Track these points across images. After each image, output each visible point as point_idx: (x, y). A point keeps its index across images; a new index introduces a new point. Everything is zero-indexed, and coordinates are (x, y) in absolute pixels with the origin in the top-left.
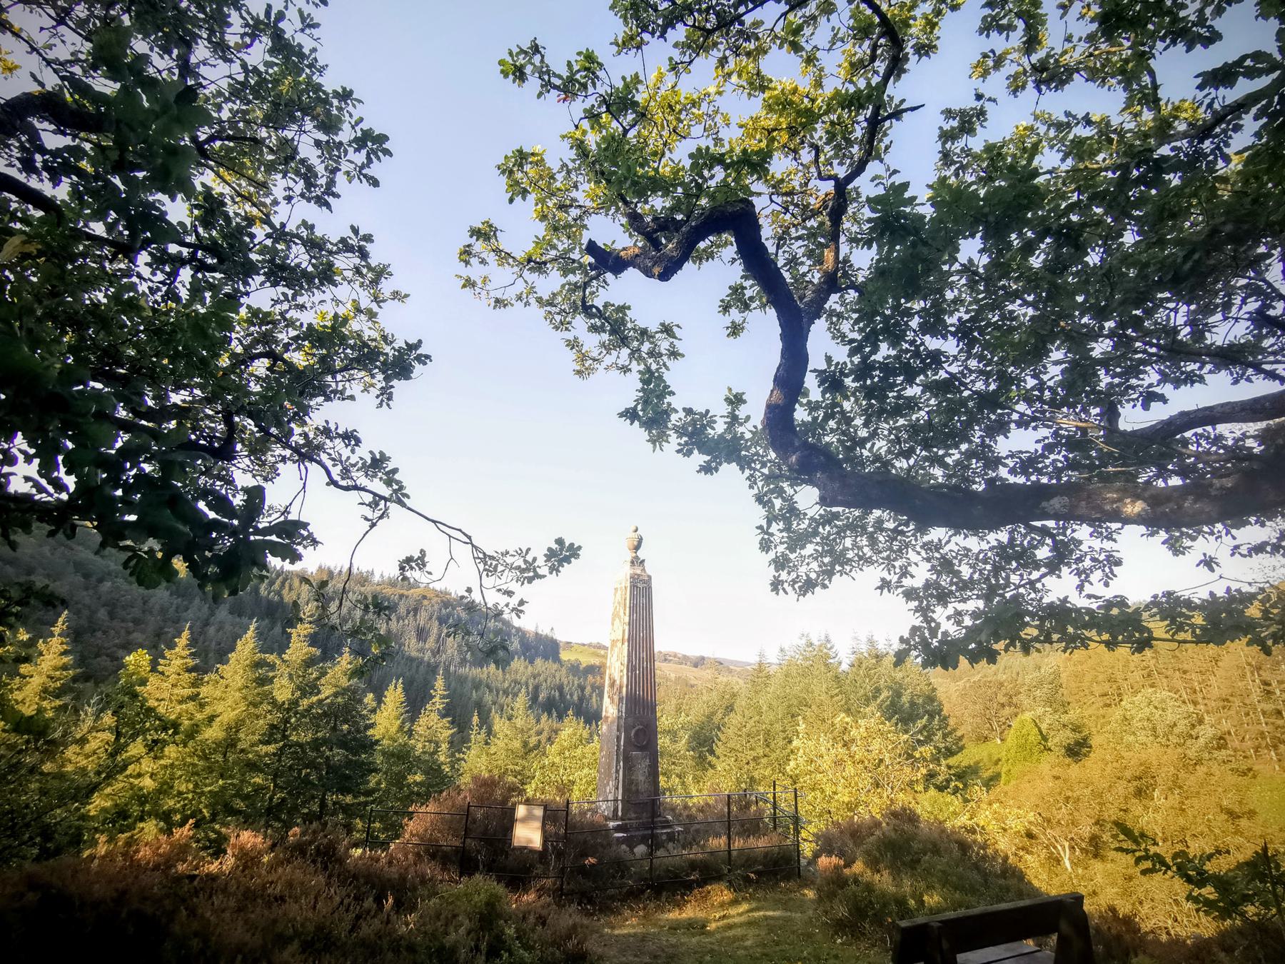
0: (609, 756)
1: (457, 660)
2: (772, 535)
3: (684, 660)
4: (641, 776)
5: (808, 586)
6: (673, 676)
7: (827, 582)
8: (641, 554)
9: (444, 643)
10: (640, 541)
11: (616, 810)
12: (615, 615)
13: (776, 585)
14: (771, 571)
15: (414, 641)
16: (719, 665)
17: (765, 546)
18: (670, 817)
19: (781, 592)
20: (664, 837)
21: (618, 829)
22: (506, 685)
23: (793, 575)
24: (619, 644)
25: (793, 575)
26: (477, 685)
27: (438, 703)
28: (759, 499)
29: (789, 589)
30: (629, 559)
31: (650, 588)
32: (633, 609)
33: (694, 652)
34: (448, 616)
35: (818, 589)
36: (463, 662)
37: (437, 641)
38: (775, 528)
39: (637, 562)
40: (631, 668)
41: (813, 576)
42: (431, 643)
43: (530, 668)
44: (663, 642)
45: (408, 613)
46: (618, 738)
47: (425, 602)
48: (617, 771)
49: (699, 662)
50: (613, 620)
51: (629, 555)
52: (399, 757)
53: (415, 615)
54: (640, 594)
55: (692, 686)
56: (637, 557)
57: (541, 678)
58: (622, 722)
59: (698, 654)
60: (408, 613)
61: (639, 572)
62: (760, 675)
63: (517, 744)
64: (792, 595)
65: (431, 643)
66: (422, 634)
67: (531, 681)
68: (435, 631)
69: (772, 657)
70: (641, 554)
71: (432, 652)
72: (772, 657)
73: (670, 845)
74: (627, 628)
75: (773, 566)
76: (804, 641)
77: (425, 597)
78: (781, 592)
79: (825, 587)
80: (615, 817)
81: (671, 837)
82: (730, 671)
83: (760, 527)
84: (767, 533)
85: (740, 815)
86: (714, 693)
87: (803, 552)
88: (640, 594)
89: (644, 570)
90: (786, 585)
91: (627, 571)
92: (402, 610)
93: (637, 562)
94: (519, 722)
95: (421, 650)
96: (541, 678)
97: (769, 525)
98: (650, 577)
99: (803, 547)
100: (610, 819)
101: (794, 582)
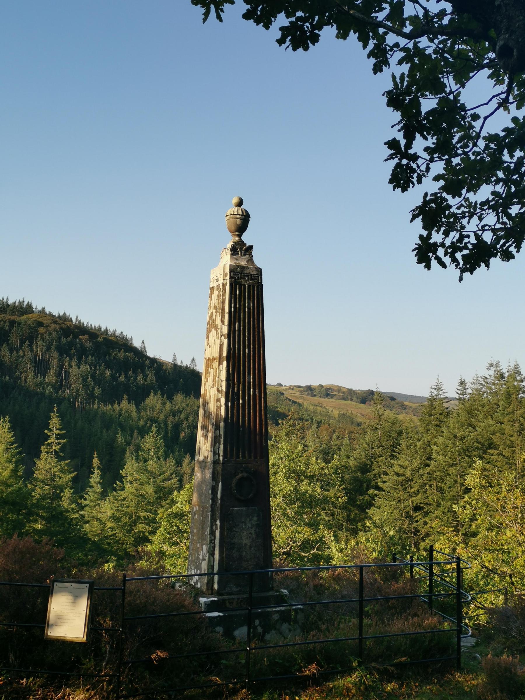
0: (202, 512)
1: (83, 395)
2: (415, 158)
3: (349, 394)
4: (245, 537)
5: (478, 256)
6: (336, 413)
7: (513, 249)
8: (247, 238)
9: (67, 373)
10: (246, 218)
11: (210, 583)
12: (211, 325)
13: (425, 253)
14: (418, 228)
15: (31, 374)
16: (391, 400)
17: (402, 179)
18: (285, 591)
19: (434, 263)
20: (276, 617)
21: (211, 607)
22: (142, 423)
23: (454, 236)
24: (215, 364)
25: (454, 236)
26: (109, 423)
27: (54, 443)
28: (394, 99)
29: (447, 260)
30: (230, 245)
31: (260, 286)
32: (234, 317)
33: (361, 385)
34: (70, 345)
35: (495, 262)
36: (91, 397)
37: (59, 374)
38: (420, 145)
39: (241, 249)
40: (231, 394)
41: (488, 237)
42: (51, 377)
43: (168, 405)
44: (285, 368)
45: (22, 342)
46: (214, 490)
47: (42, 330)
48: (213, 533)
49: (367, 397)
50: (209, 331)
51: (230, 240)
52: (14, 504)
53: (31, 345)
54: (246, 292)
55: (359, 424)
56: (241, 243)
57: (183, 416)
58: (219, 468)
59: (366, 388)
60: (22, 342)
61: (243, 263)
62: (434, 411)
63: (149, 490)
64: (453, 271)
65: (51, 377)
66: (41, 367)
67: (170, 419)
68: (55, 362)
69: (451, 391)
70: (247, 238)
71: (54, 387)
72: (451, 391)
73: (285, 627)
74: (225, 341)
75: (419, 221)
76: (492, 372)
77: (40, 324)
78: (434, 263)
79: (508, 256)
80: (210, 591)
81: (285, 617)
82: (404, 407)
83: (393, 144)
84: (405, 155)
85: (382, 590)
86: (380, 433)
87: (473, 197)
88: (246, 292)
89: (251, 261)
90: (441, 252)
91: (226, 260)
92: (15, 339)
93: (241, 249)
94: (152, 465)
95: (40, 384)
96: (183, 416)
97: (410, 139)
98: (259, 271)
99: (474, 188)
100: (203, 594)
101: (455, 248)
